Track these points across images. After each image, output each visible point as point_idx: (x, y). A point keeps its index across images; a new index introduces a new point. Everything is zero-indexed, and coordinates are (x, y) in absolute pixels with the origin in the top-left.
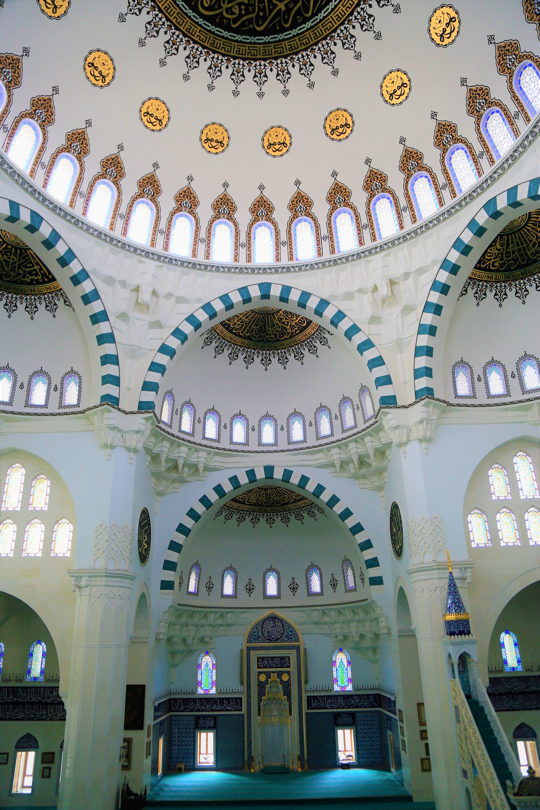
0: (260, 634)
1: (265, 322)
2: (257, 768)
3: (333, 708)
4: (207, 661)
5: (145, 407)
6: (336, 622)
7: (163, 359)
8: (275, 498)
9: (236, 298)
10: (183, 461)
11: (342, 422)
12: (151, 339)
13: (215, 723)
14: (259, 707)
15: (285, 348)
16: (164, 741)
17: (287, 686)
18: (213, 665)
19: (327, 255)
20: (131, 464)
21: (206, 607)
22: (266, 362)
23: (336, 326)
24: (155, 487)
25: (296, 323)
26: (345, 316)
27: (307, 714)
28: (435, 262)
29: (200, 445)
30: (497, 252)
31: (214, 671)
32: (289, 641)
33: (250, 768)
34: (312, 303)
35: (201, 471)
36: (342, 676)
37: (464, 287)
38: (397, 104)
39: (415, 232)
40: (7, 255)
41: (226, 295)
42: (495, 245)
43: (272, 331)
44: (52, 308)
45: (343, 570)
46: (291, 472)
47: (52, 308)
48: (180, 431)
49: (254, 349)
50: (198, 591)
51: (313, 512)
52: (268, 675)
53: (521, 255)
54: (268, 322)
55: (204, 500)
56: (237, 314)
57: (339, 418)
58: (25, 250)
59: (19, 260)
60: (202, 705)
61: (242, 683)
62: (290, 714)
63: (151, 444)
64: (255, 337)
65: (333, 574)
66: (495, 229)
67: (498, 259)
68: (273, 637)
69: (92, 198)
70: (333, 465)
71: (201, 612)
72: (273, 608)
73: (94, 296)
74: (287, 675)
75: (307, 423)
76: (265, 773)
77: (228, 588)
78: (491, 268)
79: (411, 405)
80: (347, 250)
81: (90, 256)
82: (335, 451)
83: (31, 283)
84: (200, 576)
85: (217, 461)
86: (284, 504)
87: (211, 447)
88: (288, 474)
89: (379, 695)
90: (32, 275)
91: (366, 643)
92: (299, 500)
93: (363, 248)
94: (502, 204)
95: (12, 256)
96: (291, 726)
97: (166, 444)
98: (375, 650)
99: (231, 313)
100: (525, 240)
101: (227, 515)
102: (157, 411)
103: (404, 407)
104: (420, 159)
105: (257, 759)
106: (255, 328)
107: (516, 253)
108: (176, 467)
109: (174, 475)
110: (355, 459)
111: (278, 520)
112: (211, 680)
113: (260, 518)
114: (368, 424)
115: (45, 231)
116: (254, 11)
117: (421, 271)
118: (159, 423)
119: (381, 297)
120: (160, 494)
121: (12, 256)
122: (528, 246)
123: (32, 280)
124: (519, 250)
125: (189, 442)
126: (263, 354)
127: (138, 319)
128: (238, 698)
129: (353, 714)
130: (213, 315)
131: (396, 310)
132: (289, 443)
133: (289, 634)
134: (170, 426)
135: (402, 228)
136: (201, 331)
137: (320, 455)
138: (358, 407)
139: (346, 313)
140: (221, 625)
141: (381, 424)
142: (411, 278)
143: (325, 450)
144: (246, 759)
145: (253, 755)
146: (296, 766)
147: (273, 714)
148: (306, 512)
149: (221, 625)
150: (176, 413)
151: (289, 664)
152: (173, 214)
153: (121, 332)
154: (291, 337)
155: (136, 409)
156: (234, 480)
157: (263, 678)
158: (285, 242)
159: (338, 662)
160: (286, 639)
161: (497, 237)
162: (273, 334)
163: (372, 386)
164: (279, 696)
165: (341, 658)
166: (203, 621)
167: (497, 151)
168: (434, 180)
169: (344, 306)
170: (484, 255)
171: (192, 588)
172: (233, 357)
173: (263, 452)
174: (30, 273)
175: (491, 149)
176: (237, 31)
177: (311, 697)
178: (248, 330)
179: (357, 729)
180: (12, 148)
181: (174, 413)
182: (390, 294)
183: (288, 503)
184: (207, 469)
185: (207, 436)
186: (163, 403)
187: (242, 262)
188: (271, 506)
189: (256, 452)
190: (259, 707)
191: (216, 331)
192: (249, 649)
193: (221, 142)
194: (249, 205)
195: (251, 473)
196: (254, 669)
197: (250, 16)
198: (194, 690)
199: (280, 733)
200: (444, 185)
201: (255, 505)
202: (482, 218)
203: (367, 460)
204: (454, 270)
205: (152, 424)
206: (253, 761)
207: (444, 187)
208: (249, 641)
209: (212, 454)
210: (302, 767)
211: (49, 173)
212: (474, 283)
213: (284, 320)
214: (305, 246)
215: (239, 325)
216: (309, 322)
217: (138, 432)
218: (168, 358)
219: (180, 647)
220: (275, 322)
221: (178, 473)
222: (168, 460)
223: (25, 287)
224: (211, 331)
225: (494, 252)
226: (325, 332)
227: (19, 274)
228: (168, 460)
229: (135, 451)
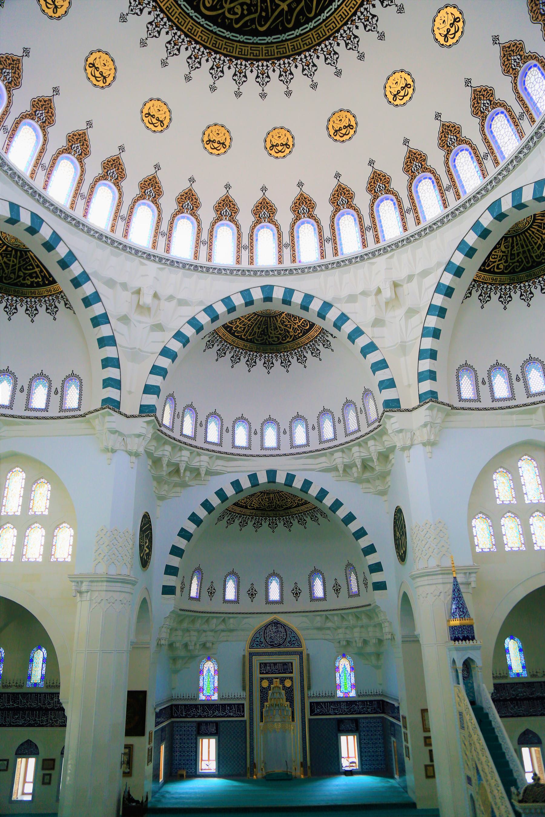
0: (262, 640)
1: (268, 324)
2: (259, 774)
3: (336, 714)
4: (209, 666)
5: (146, 410)
6: (339, 628)
7: (164, 362)
8: (278, 502)
9: (238, 301)
10: (184, 465)
11: (345, 425)
12: (152, 342)
13: (217, 729)
14: (262, 713)
15: (288, 351)
16: (165, 748)
17: (289, 692)
18: (215, 671)
19: (330, 257)
20: (132, 468)
21: (208, 613)
22: (268, 365)
23: (339, 329)
24: (157, 492)
25: (298, 326)
26: (348, 319)
27: (310, 720)
28: (439, 264)
29: (202, 448)
30: (501, 254)
31: (216, 677)
32: (292, 646)
33: (252, 775)
34: (315, 306)
35: (203, 475)
36: (345, 682)
37: (469, 290)
38: (401, 105)
39: (419, 234)
40: (7, 257)
41: (229, 298)
42: (500, 247)
43: (275, 334)
44: (52, 310)
45: (346, 574)
46: (294, 476)
47: (52, 310)
48: (182, 434)
49: (256, 352)
50: (200, 596)
51: (316, 517)
52: (271, 681)
53: (526, 257)
54: (270, 325)
55: (206, 505)
56: (239, 317)
57: (342, 422)
58: (26, 252)
59: (19, 263)
60: (203, 711)
61: (244, 689)
62: (293, 720)
63: (153, 448)
64: (257, 340)
65: (336, 579)
66: (500, 231)
67: (503, 261)
68: (276, 642)
69: (93, 200)
70: (336, 469)
71: (202, 617)
72: (275, 613)
73: (95, 298)
74: (290, 681)
75: (310, 427)
76: (267, 780)
77: (231, 593)
78: (496, 270)
79: (414, 409)
80: (350, 252)
81: (91, 258)
82: (338, 455)
83: (31, 285)
84: (201, 581)
85: (219, 465)
86: (287, 508)
87: (213, 451)
88: (290, 478)
89: (383, 701)
90: (32, 278)
91: (370, 649)
92: (302, 504)
93: (366, 250)
94: (507, 205)
95: (12, 259)
96: (293, 732)
97: (168, 448)
98: (378, 655)
99: (233, 316)
100: (530, 242)
101: (229, 520)
102: (159, 414)
103: (408, 410)
104: (424, 160)
105: (260, 765)
106: (257, 331)
107: (521, 256)
108: (177, 471)
109: (176, 479)
110: (359, 463)
111: (281, 525)
112: (213, 685)
113: (263, 523)
114: (371, 428)
115: (45, 233)
116: (256, 11)
117: (425, 273)
118: (160, 427)
119: (384, 300)
120: (162, 498)
121: (12, 259)
122: (533, 248)
123: (32, 282)
124: (524, 252)
125: (191, 445)
126: (265, 357)
127: (140, 322)
128: (240, 704)
129: (356, 720)
130: (215, 318)
131: (400, 312)
132: (292, 447)
133: (292, 640)
134: (172, 430)
135: (405, 230)
136: (203, 333)
137: (323, 459)
138: (361, 410)
139: (349, 315)
140: (223, 631)
141: (385, 428)
142: (415, 280)
143: (328, 454)
144: (248, 766)
145: (255, 761)
146: (299, 773)
147: (276, 720)
148: (309, 517)
149: (223, 631)
150: (178, 416)
151: (292, 669)
152: (174, 216)
153: (123, 335)
154: (293, 340)
155: (137, 413)
156: (236, 484)
157: (265, 684)
158: (287, 244)
159: (341, 668)
160: (289, 644)
161: (502, 239)
162: (275, 337)
163: (375, 389)
164: (281, 702)
165: (344, 664)
166: (205, 627)
167: (502, 153)
168: (438, 181)
169: (347, 309)
170: (488, 257)
171: (194, 593)
172: (235, 360)
173: (265, 456)
174: (31, 276)
175: (495, 151)
176: (240, 31)
177: (313, 703)
178: (251, 333)
179: (360, 735)
180: (12, 149)
181: (176, 417)
182: (394, 296)
183: (290, 508)
184: (209, 473)
185: (209, 439)
186: (165, 406)
187: (245, 264)
188: (274, 510)
189: (258, 456)
190: (262, 713)
191: (218, 334)
192: (251, 655)
193: (223, 144)
194: (252, 206)
195: (253, 478)
196: (257, 675)
197: (252, 16)
198: (195, 696)
199: (283, 739)
200: (448, 186)
201: (257, 509)
202: (487, 220)
203: (370, 464)
204: (459, 272)
205: (154, 428)
206: (255, 768)
207: (448, 189)
208: (251, 647)
209: (214, 458)
210: (305, 773)
211: (49, 175)
212: (479, 286)
213: (287, 323)
214: (308, 248)
215: (241, 327)
216: (312, 325)
217: (139, 436)
218: (170, 361)
219: (182, 653)
220: (278, 325)
221: (180, 478)
222: (169, 464)
223: (25, 290)
224: (213, 333)
225: (499, 254)
226: (328, 334)
227: (19, 277)
228: (169, 464)
229: (137, 455)
